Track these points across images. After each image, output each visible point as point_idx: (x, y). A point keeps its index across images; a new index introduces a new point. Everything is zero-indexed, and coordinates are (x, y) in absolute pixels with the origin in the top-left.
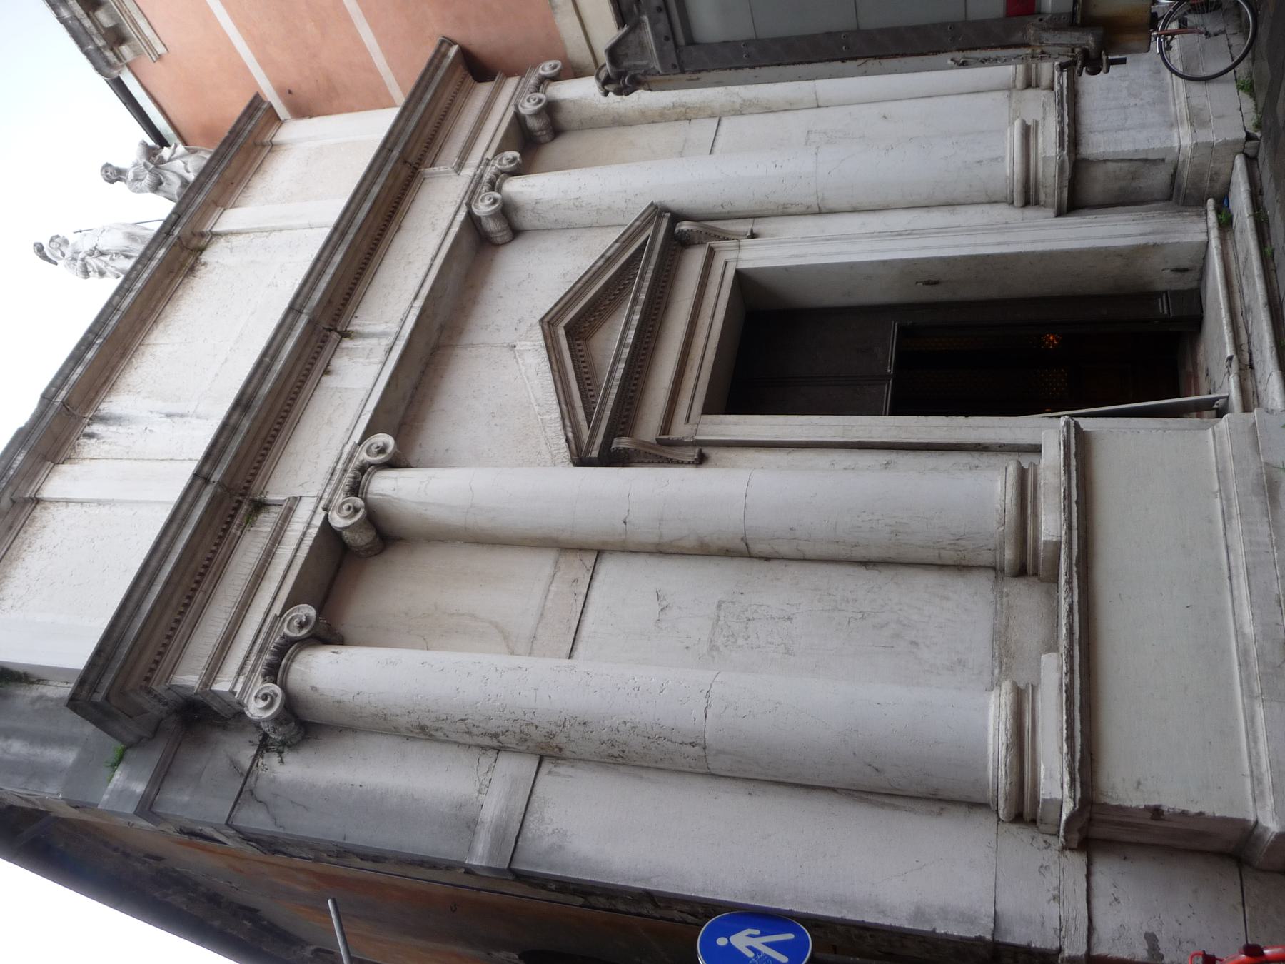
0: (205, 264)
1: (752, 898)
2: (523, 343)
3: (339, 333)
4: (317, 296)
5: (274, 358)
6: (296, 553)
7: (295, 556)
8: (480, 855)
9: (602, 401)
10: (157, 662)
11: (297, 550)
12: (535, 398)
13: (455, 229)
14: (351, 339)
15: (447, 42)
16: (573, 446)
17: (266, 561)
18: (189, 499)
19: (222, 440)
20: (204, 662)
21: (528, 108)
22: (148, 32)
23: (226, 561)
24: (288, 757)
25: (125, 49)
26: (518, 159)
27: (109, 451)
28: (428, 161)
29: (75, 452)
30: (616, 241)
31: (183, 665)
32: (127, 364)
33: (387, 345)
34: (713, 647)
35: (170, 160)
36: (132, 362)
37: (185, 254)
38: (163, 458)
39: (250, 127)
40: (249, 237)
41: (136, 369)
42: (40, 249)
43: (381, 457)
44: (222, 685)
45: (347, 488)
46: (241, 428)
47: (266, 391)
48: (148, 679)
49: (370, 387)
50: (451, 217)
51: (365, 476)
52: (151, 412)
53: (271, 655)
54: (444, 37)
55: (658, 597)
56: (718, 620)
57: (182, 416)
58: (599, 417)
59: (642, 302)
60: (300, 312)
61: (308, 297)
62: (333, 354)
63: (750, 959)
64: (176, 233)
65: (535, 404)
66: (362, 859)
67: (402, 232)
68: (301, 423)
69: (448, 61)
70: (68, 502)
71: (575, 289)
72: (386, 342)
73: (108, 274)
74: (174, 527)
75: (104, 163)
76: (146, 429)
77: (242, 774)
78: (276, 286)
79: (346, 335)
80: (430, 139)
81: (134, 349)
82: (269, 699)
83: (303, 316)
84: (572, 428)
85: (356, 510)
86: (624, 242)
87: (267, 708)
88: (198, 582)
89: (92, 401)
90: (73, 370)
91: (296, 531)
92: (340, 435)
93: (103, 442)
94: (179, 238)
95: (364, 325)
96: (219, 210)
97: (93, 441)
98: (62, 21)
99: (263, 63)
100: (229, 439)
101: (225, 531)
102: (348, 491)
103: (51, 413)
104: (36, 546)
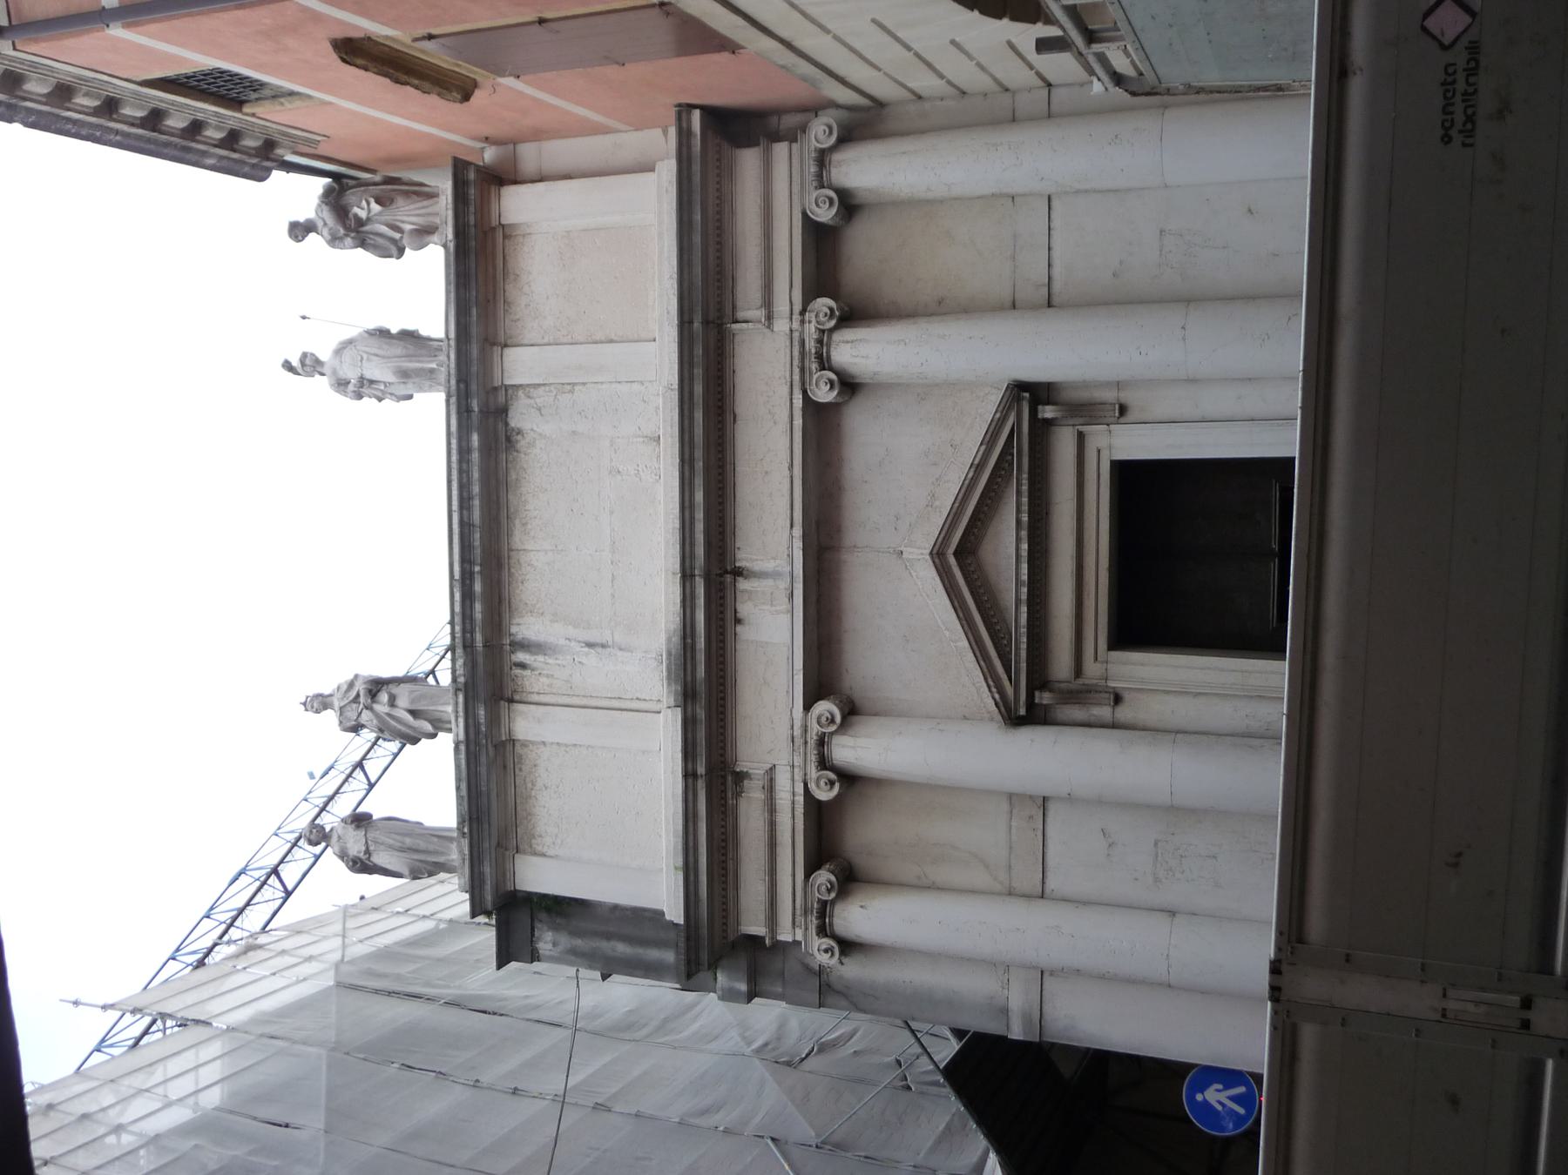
0: (519, 432)
2: (909, 549)
3: (730, 573)
4: (700, 551)
8: (1016, 1033)
10: (725, 924)
13: (798, 422)
14: (746, 578)
15: (684, 109)
16: (1003, 709)
17: (772, 830)
19: (690, 735)
20: (762, 917)
27: (552, 684)
28: (728, 311)
30: (981, 444)
31: (744, 918)
33: (786, 589)
34: (1157, 880)
35: (368, 219)
36: (513, 574)
37: (491, 420)
39: (472, 219)
40: (550, 391)
42: (288, 366)
43: (833, 728)
44: (785, 936)
45: (816, 764)
46: (698, 717)
50: (788, 404)
52: (569, 639)
54: (679, 105)
57: (603, 646)
60: (693, 576)
65: (944, 629)
67: (740, 425)
71: (954, 510)
72: (783, 584)
75: (286, 227)
77: (815, 973)
78: (619, 472)
83: (697, 578)
84: (996, 687)
85: (832, 783)
87: (833, 955)
93: (540, 674)
94: (481, 411)
95: (752, 560)
96: (497, 350)
97: (527, 673)
100: (694, 732)
101: (725, 805)
103: (480, 660)
104: (540, 783)
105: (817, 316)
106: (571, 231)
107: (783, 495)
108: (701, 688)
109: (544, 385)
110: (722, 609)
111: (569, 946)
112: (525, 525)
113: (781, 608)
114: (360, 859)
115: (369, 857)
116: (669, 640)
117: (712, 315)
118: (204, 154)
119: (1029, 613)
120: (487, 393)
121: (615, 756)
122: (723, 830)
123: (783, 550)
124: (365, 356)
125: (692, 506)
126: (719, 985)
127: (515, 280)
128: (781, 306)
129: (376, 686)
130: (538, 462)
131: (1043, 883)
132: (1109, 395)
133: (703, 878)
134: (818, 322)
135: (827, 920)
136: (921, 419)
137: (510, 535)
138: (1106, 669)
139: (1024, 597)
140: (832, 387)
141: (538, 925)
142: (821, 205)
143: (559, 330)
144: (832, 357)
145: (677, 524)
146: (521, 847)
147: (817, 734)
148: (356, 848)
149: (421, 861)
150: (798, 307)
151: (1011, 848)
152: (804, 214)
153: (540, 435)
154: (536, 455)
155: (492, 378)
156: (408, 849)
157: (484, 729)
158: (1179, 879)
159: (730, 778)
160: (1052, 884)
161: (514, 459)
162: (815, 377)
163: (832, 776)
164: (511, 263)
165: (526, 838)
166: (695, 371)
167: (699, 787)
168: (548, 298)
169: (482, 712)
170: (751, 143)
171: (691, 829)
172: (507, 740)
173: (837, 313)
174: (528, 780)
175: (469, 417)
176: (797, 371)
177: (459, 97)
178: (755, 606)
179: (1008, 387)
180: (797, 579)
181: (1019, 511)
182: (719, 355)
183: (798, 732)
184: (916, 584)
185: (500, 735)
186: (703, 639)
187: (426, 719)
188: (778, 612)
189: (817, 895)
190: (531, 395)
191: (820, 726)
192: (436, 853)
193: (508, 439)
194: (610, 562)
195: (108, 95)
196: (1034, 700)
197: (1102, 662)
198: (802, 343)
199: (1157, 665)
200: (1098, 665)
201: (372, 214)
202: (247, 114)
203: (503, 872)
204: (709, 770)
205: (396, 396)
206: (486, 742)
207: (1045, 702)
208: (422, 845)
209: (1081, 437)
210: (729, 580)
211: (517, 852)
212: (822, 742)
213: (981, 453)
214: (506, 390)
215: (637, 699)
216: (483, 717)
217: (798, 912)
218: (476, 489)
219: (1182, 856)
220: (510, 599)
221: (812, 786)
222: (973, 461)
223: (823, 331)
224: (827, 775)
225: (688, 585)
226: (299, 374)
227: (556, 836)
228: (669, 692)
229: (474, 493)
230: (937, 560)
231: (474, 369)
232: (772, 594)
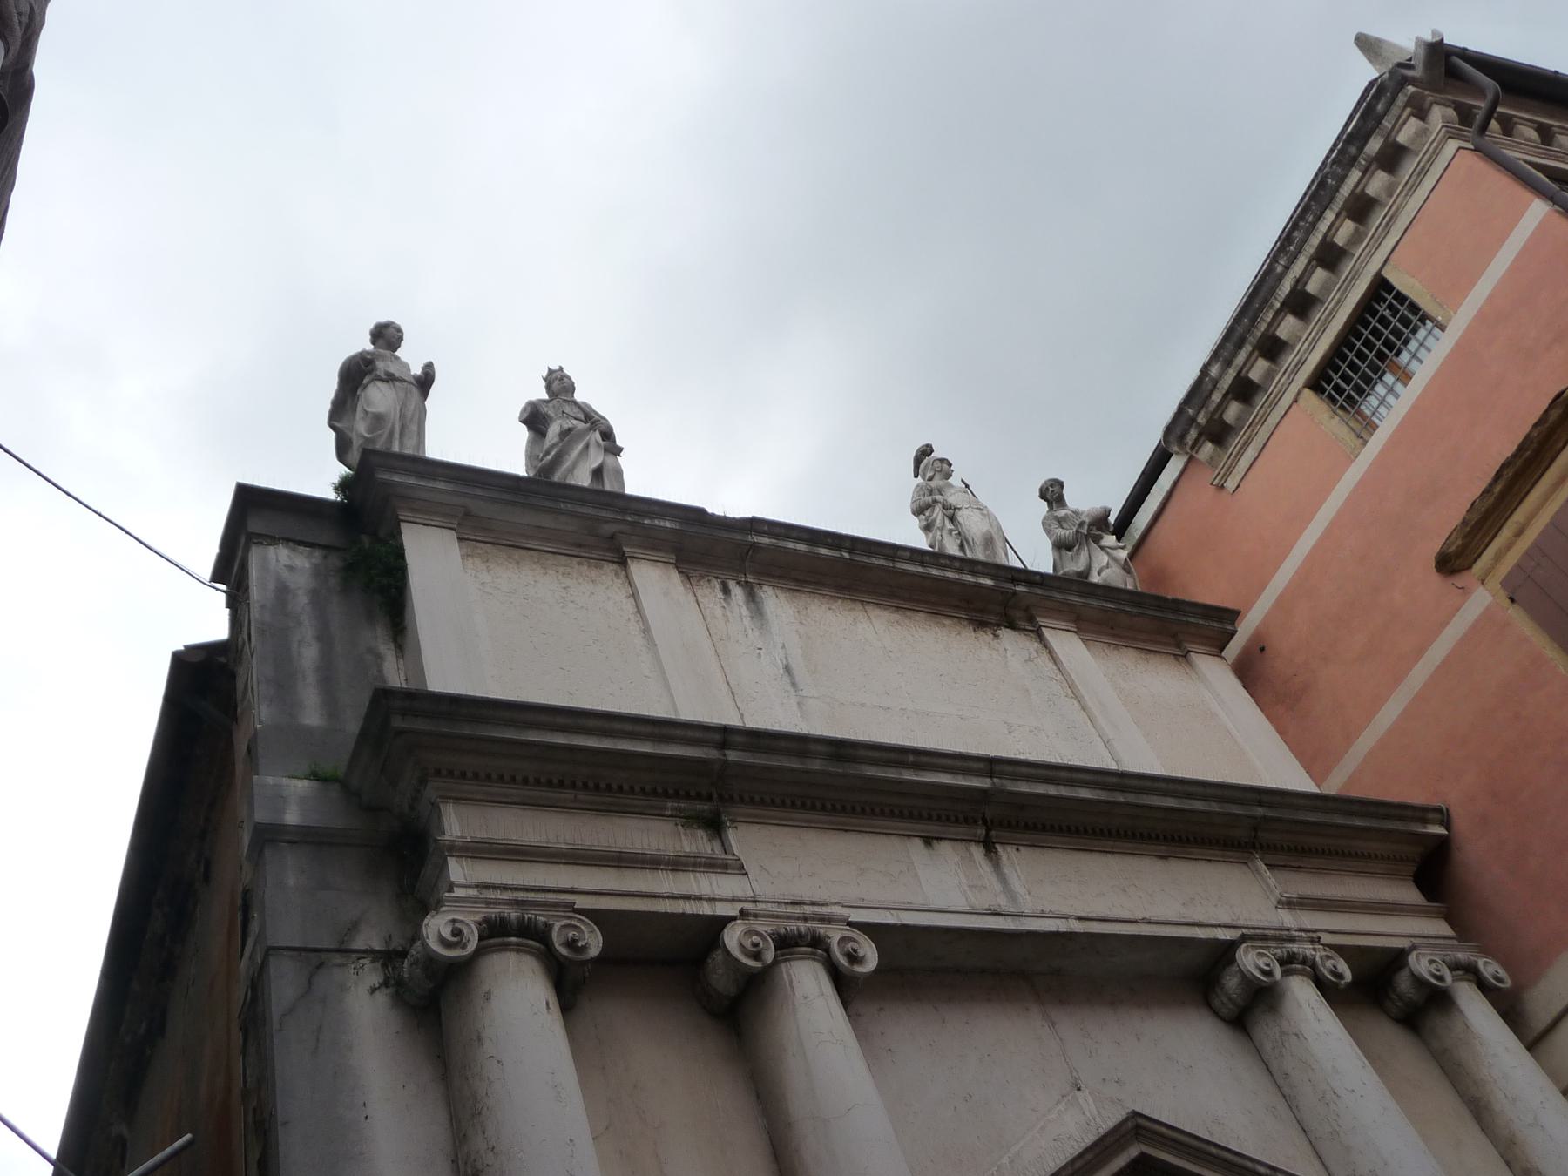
3: (987, 834)
4: (1023, 787)
6: (668, 897)
7: (663, 897)
10: (463, 775)
11: (673, 897)
14: (985, 855)
17: (643, 862)
18: (690, 734)
19: (783, 744)
20: (481, 835)
21: (1421, 964)
22: (1244, 463)
23: (625, 811)
24: (382, 998)
25: (1208, 448)
26: (1343, 982)
27: (716, 618)
35: (1102, 548)
36: (836, 602)
38: (731, 683)
41: (830, 609)
44: (457, 870)
45: (783, 931)
48: (438, 772)
49: (933, 907)
51: (809, 949)
52: (783, 647)
53: (518, 917)
54: (1447, 810)
57: (794, 684)
60: (991, 775)
61: (1016, 777)
62: (956, 840)
66: (259, 1160)
67: (1159, 865)
70: (634, 595)
72: (1003, 903)
73: (931, 535)
76: (760, 649)
79: (989, 848)
80: (1303, 848)
81: (853, 598)
82: (456, 939)
83: (988, 780)
85: (757, 956)
88: (585, 786)
89: (769, 575)
90: (798, 540)
93: (724, 607)
94: (1015, 593)
96: (1072, 626)
97: (720, 595)
98: (1205, 370)
99: (1282, 604)
101: (666, 795)
102: (779, 934)
103: (738, 537)
104: (568, 582)
111: (292, 586)
120: (1027, 609)
126: (285, 781)
135: (513, 939)
141: (318, 553)
144: (1291, 978)
149: (391, 434)
155: (1045, 617)
157: (646, 522)
161: (964, 626)
165: (479, 551)
202: (1299, 393)
210: (979, 832)
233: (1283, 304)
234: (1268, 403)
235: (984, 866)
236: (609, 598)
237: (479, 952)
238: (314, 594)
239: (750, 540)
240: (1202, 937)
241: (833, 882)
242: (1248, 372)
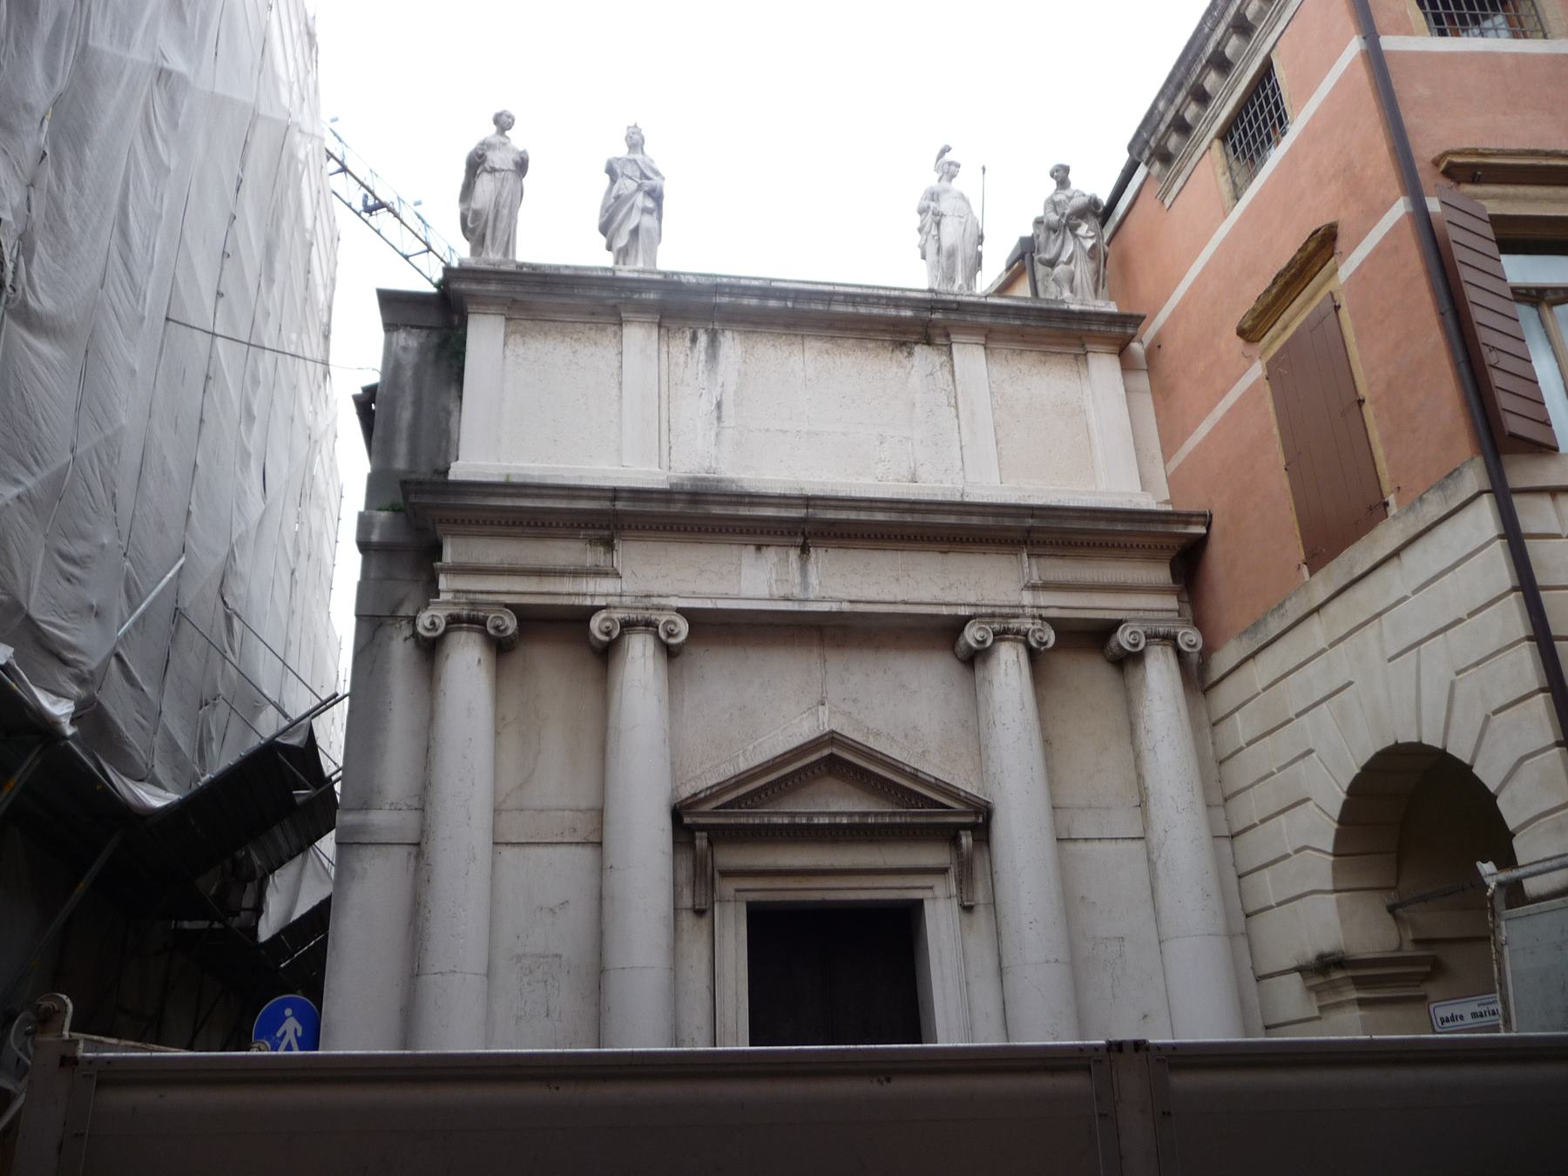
0: (910, 354)
1: (326, 1026)
3: (804, 541)
4: (831, 515)
5: (751, 504)
6: (566, 595)
7: (563, 595)
9: (743, 813)
10: (455, 522)
11: (569, 594)
12: (763, 742)
13: (945, 611)
14: (799, 557)
16: (689, 801)
17: (556, 573)
18: (592, 494)
19: (655, 496)
20: (463, 559)
24: (411, 642)
25: (1157, 166)
29: (674, 333)
30: (936, 779)
31: (460, 542)
32: (778, 334)
33: (792, 594)
34: (519, 958)
36: (781, 338)
38: (672, 420)
39: (1094, 327)
40: (948, 386)
42: (946, 150)
43: (663, 635)
44: (443, 582)
46: (672, 505)
47: (714, 512)
48: (441, 521)
49: (743, 596)
51: (644, 628)
54: (1211, 516)
55: (563, 904)
56: (544, 957)
57: (719, 418)
58: (726, 815)
59: (865, 821)
60: (807, 507)
62: (781, 546)
63: (275, 1034)
64: (937, 316)
67: (938, 557)
68: (700, 545)
69: (1180, 529)
72: (797, 592)
74: (565, 492)
75: (1065, 162)
77: (393, 612)
78: (881, 443)
79: (805, 550)
85: (608, 633)
86: (939, 786)
88: (529, 525)
91: (587, 587)
92: (688, 587)
93: (687, 355)
94: (931, 320)
96: (982, 340)
97: (688, 343)
99: (1174, 315)
103: (704, 300)
104: (577, 346)
105: (1039, 630)
106: (1085, 413)
107: (878, 594)
108: (700, 510)
109: (954, 381)
110: (772, 533)
112: (827, 352)
113: (775, 590)
114: (483, 162)
115: (487, 171)
116: (732, 481)
117: (1035, 536)
118: (1171, 101)
119: (782, 825)
120: (945, 328)
121: (611, 422)
122: (554, 524)
123: (830, 593)
124: (963, 220)
125: (871, 509)
126: (375, 513)
127: (1041, 361)
128: (1045, 599)
129: (656, 195)
130: (885, 370)
131: (507, 844)
132: (980, 895)
133: (508, 502)
134: (1034, 631)
135: (465, 625)
136: (945, 723)
137: (818, 338)
138: (729, 901)
139: (797, 820)
140: (978, 642)
141: (424, 333)
142: (1132, 636)
143: (1001, 397)
144: (1003, 643)
145: (842, 494)
146: (512, 323)
147: (656, 620)
148: (495, 158)
149: (486, 222)
150: (1045, 613)
151: (542, 810)
152: (1119, 623)
153: (909, 373)
154: (891, 367)
156: (497, 211)
157: (635, 297)
158: (522, 980)
159: (606, 533)
160: (508, 853)
161: (885, 347)
162: (987, 627)
163: (615, 634)
164: (1054, 359)
166: (991, 518)
167: (602, 502)
168: (1028, 389)
169: (652, 296)
170: (1175, 575)
171: (560, 492)
172: (621, 318)
173: (1042, 648)
174: (581, 335)
175: (927, 309)
176: (989, 610)
177: (1246, 326)
178: (774, 565)
179: (988, 803)
180: (802, 605)
181: (876, 814)
182: (1000, 541)
183: (655, 601)
184: (795, 718)
185: (626, 312)
186: (748, 513)
187: (629, 241)
188: (770, 586)
189: (492, 616)
190: (943, 367)
191: (664, 623)
192: (494, 238)
193: (903, 344)
194: (799, 429)
195: (1257, 29)
196: (698, 831)
197: (735, 897)
198: (1016, 616)
199: (736, 949)
200: (733, 893)
201: (1081, 239)
202: (1211, 142)
203: (487, 303)
204: (616, 514)
205: (925, 244)
206: (622, 298)
207: (697, 842)
208: (502, 225)
209: (943, 871)
210: (798, 540)
211: (506, 319)
212: (649, 625)
213: (928, 778)
214: (945, 345)
215: (670, 448)
216: (647, 296)
217: (471, 596)
218: (863, 310)
219: (546, 982)
220: (756, 332)
221: (603, 614)
222: (921, 771)
223: (1026, 635)
224: (616, 628)
225: (800, 502)
226: (938, 160)
227: (525, 359)
228: (682, 478)
229: (859, 308)
230: (827, 737)
231: (969, 318)
232: (787, 581)
233: (1208, 62)
234: (1193, 143)
235: (794, 565)
236: (603, 357)
237: (446, 631)
238: (418, 370)
239: (714, 301)
240: (945, 613)
241: (678, 580)
242: (1184, 112)
